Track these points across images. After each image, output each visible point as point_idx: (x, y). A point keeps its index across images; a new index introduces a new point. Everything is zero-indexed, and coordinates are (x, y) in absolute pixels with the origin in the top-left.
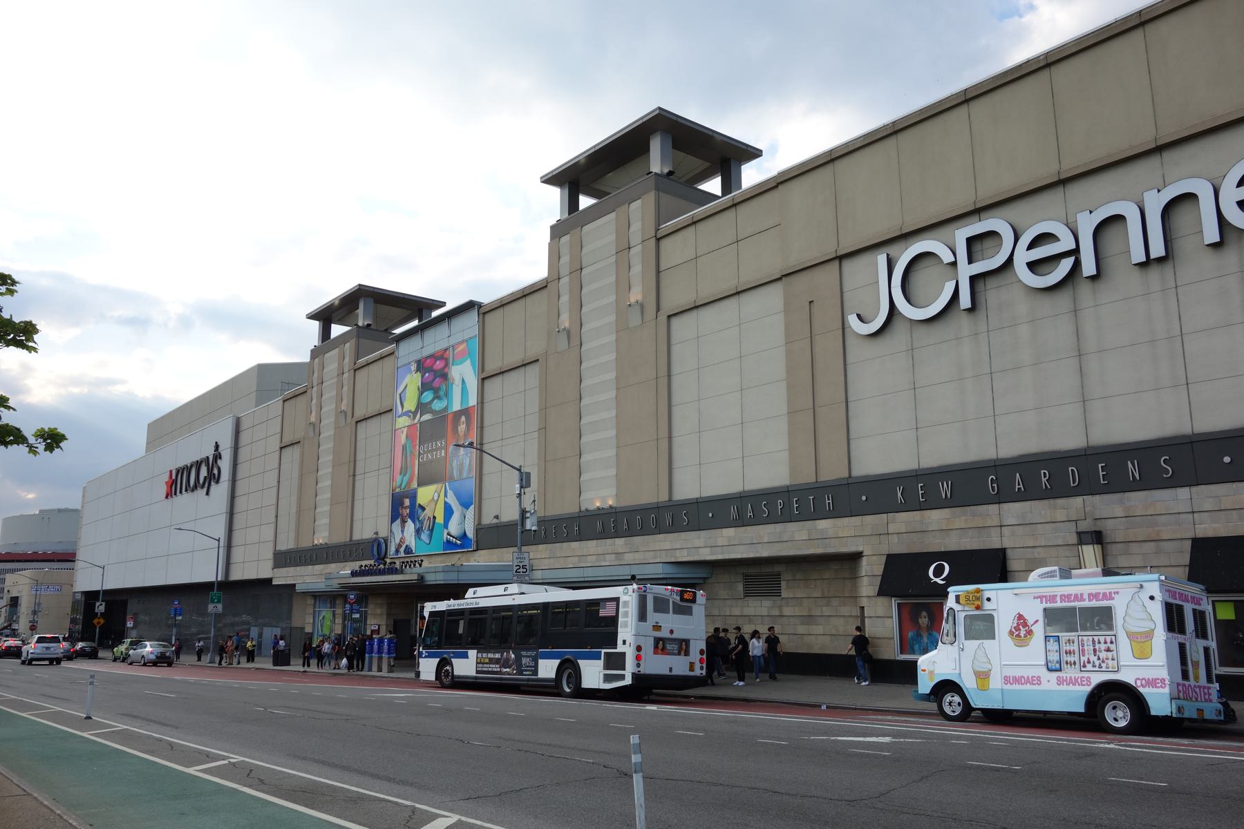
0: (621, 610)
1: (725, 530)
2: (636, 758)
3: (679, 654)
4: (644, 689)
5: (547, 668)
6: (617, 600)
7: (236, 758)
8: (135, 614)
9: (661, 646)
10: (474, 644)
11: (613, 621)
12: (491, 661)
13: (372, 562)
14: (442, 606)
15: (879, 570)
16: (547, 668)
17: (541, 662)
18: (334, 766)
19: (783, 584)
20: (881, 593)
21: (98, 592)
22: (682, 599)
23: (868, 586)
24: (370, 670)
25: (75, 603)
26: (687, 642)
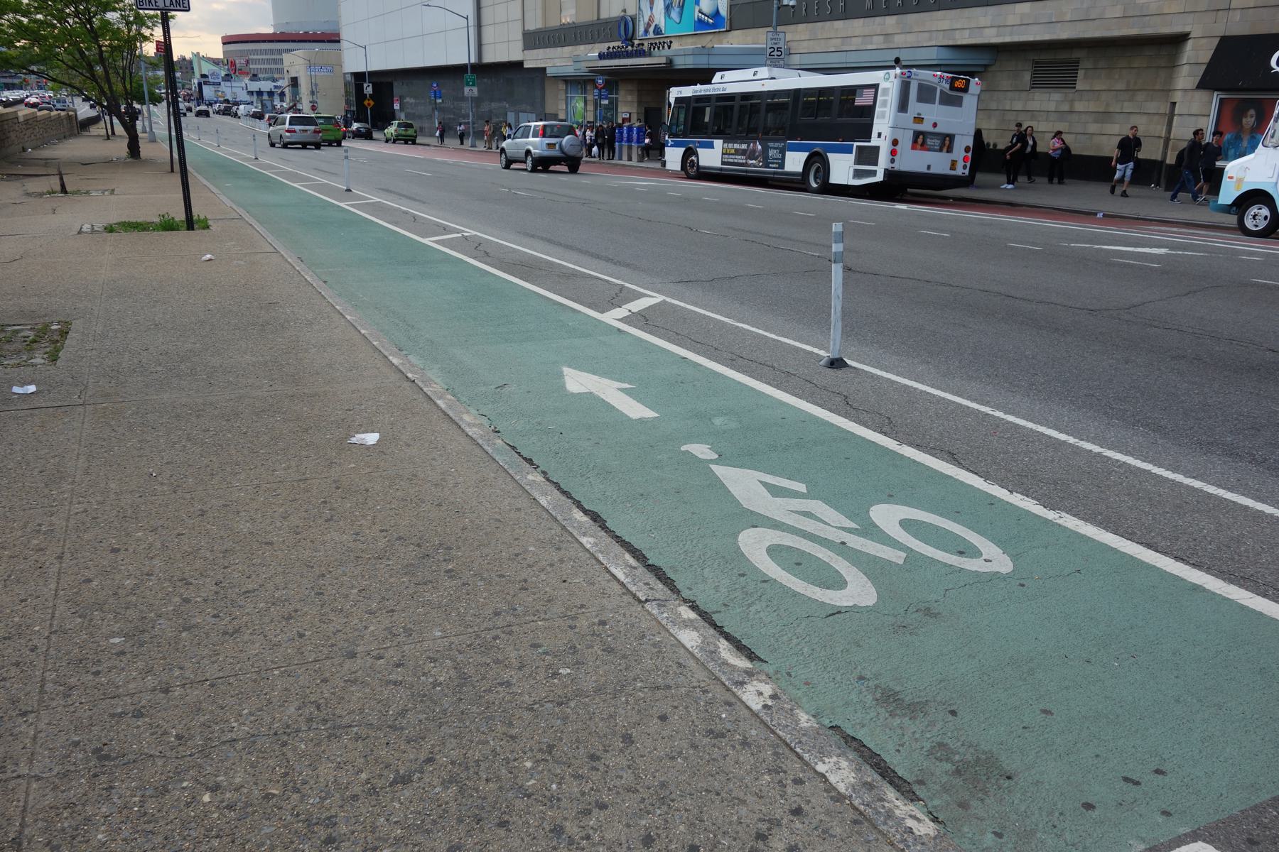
0: (879, 98)
1: (1018, 6)
2: (837, 248)
3: (941, 150)
4: (897, 187)
5: (795, 162)
6: (875, 87)
7: (470, 232)
8: (402, 98)
9: (920, 140)
10: (719, 134)
11: (869, 111)
12: (737, 152)
13: (619, 44)
14: (687, 91)
15: (1206, 56)
16: (795, 162)
17: (789, 155)
18: (569, 247)
19: (1081, 73)
20: (1202, 85)
21: (363, 74)
22: (952, 88)
23: (1186, 77)
24: (621, 159)
25: (346, 84)
26: (951, 137)
